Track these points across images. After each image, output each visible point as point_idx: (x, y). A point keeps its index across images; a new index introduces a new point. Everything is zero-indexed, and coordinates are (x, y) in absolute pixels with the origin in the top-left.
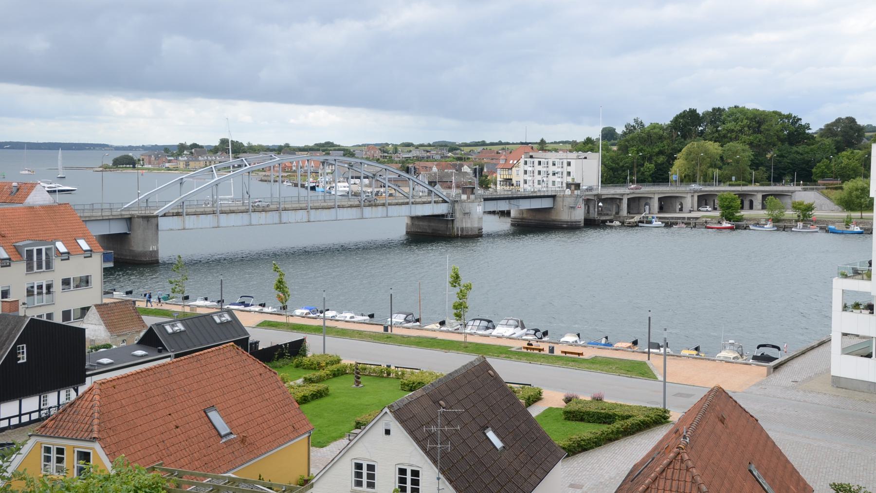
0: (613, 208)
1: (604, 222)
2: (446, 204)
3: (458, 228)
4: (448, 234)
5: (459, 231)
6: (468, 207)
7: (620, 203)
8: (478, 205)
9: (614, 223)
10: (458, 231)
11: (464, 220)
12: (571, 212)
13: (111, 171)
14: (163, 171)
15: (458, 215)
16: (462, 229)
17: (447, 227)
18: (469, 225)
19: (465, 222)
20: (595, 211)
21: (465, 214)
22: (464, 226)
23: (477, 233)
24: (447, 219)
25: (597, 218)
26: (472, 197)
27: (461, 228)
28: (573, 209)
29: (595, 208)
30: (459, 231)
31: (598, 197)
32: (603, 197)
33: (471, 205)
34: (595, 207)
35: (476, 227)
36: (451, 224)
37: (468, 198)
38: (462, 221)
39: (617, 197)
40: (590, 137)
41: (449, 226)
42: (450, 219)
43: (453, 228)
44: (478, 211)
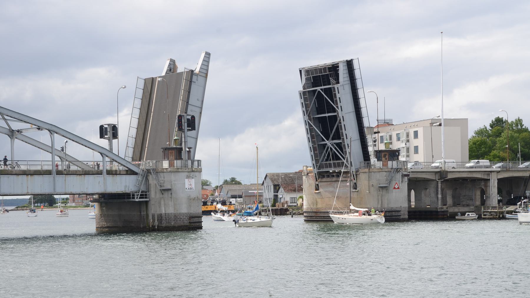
0: (475, 195)
1: (456, 214)
2: (133, 177)
3: (153, 216)
4: (142, 226)
5: (156, 221)
6: (168, 180)
7: (486, 186)
8: (188, 177)
9: (466, 215)
10: (154, 220)
11: (162, 202)
12: (382, 196)
13: (23, 210)
14: (79, 208)
15: (154, 195)
16: (160, 217)
17: (141, 215)
18: (171, 210)
19: (165, 204)
20: (438, 198)
21: (164, 191)
22: (164, 212)
23: (188, 224)
24: (133, 200)
25: (442, 208)
26: (178, 163)
27: (158, 216)
28: (384, 191)
29: (437, 194)
30: (156, 221)
31: (441, 176)
32: (450, 176)
33: (173, 177)
34: (437, 191)
35: (183, 214)
36: (145, 206)
37: (171, 165)
38: (160, 203)
39: (479, 176)
40: (500, 117)
41: (142, 213)
42: (137, 200)
43: (147, 215)
44: (187, 186)
